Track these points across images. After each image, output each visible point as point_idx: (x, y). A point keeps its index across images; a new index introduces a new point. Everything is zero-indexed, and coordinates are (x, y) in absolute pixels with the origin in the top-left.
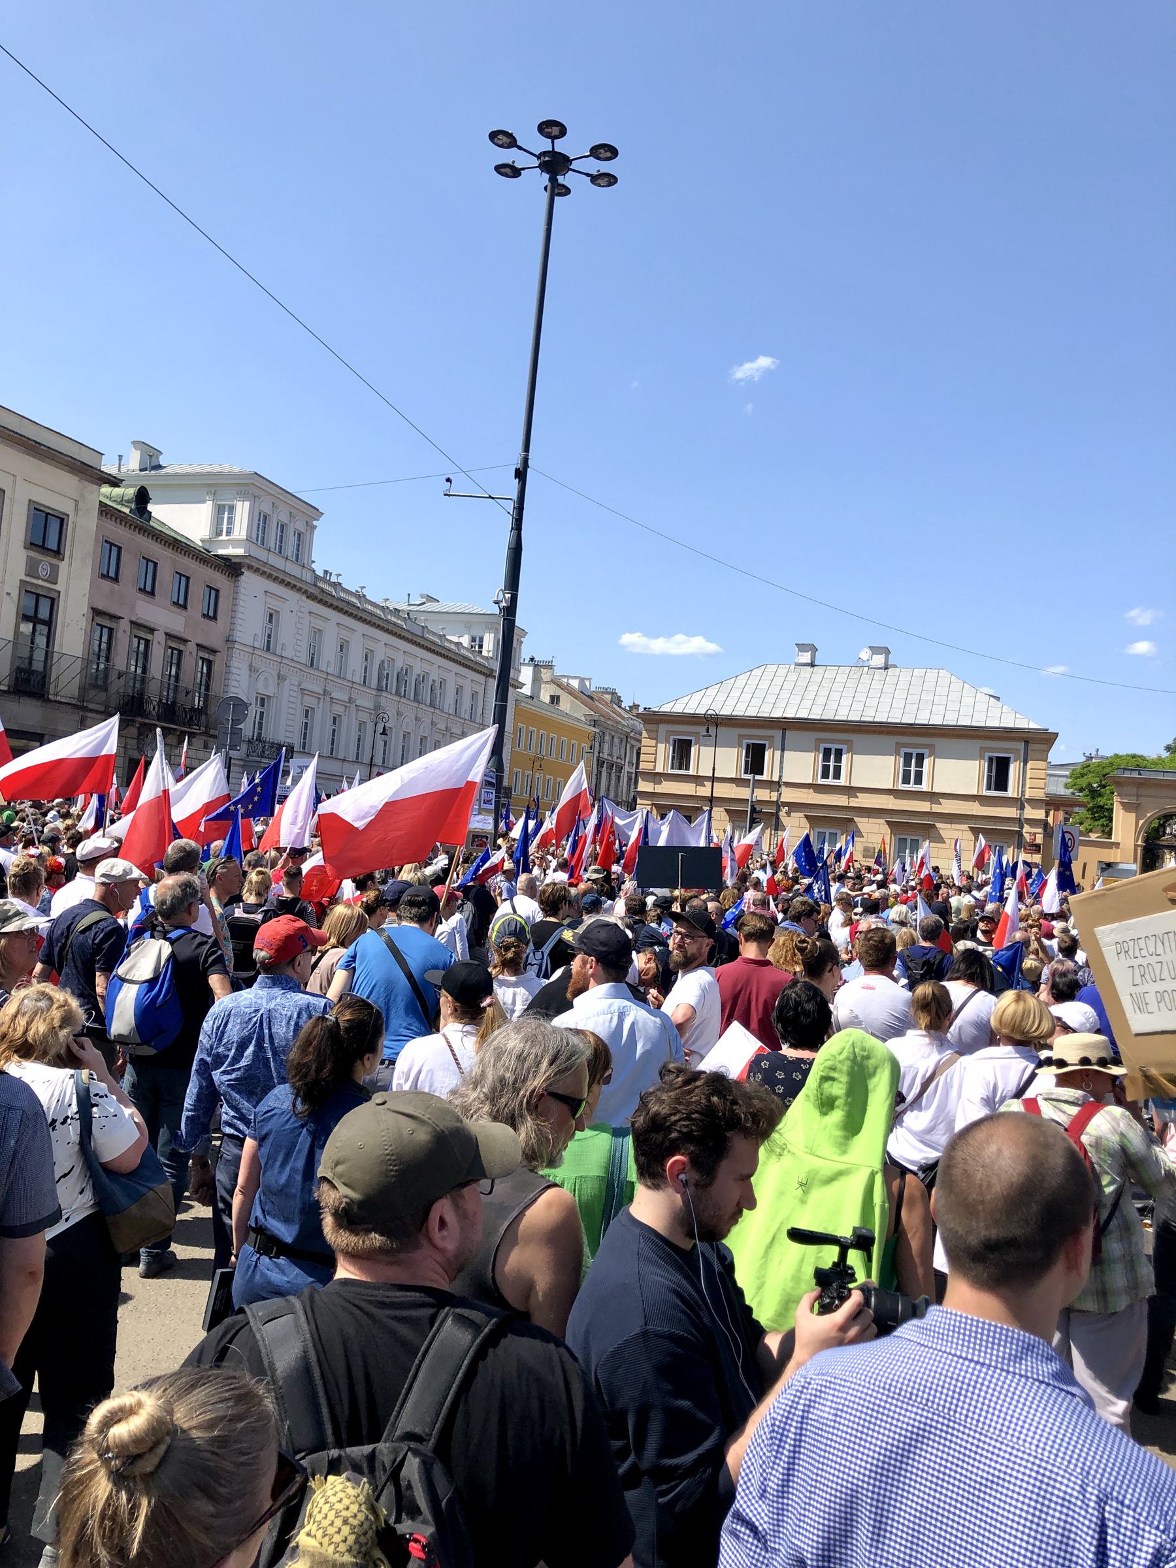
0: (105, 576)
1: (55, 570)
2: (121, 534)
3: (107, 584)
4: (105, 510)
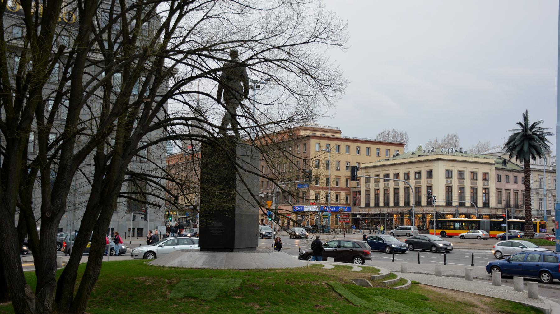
0: (498, 181)
1: (488, 183)
2: (500, 172)
3: (499, 183)
4: (496, 169)
